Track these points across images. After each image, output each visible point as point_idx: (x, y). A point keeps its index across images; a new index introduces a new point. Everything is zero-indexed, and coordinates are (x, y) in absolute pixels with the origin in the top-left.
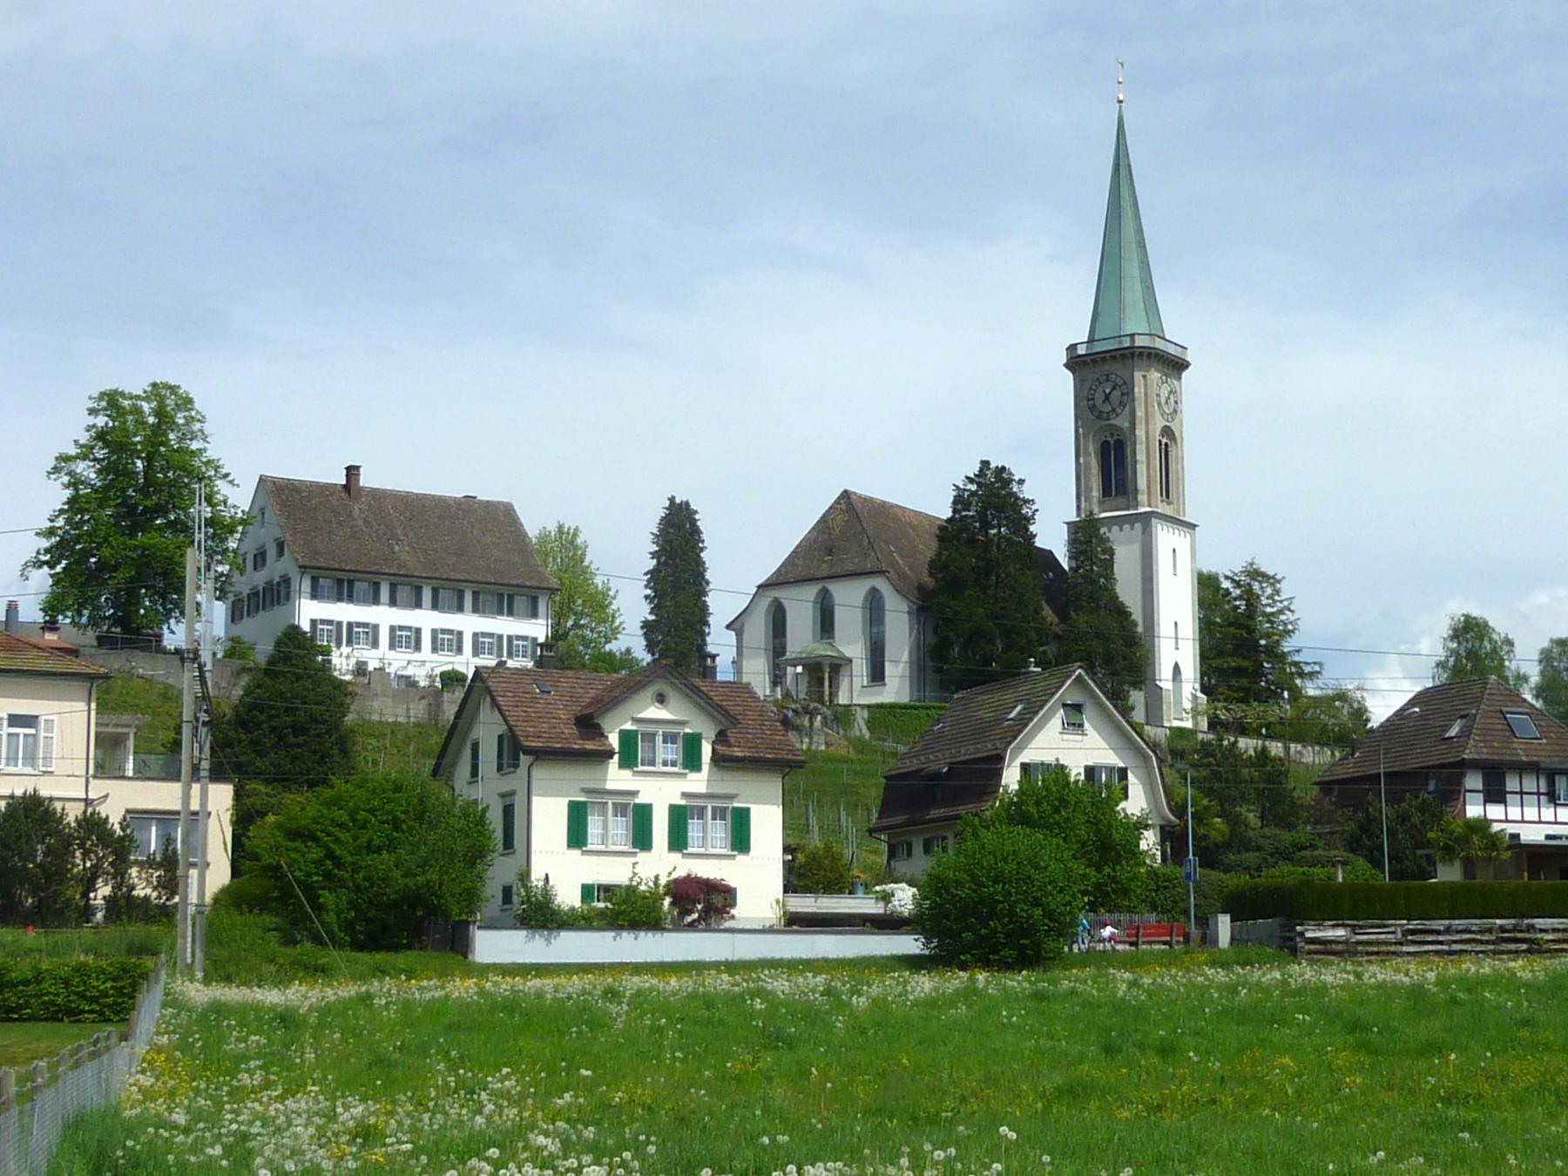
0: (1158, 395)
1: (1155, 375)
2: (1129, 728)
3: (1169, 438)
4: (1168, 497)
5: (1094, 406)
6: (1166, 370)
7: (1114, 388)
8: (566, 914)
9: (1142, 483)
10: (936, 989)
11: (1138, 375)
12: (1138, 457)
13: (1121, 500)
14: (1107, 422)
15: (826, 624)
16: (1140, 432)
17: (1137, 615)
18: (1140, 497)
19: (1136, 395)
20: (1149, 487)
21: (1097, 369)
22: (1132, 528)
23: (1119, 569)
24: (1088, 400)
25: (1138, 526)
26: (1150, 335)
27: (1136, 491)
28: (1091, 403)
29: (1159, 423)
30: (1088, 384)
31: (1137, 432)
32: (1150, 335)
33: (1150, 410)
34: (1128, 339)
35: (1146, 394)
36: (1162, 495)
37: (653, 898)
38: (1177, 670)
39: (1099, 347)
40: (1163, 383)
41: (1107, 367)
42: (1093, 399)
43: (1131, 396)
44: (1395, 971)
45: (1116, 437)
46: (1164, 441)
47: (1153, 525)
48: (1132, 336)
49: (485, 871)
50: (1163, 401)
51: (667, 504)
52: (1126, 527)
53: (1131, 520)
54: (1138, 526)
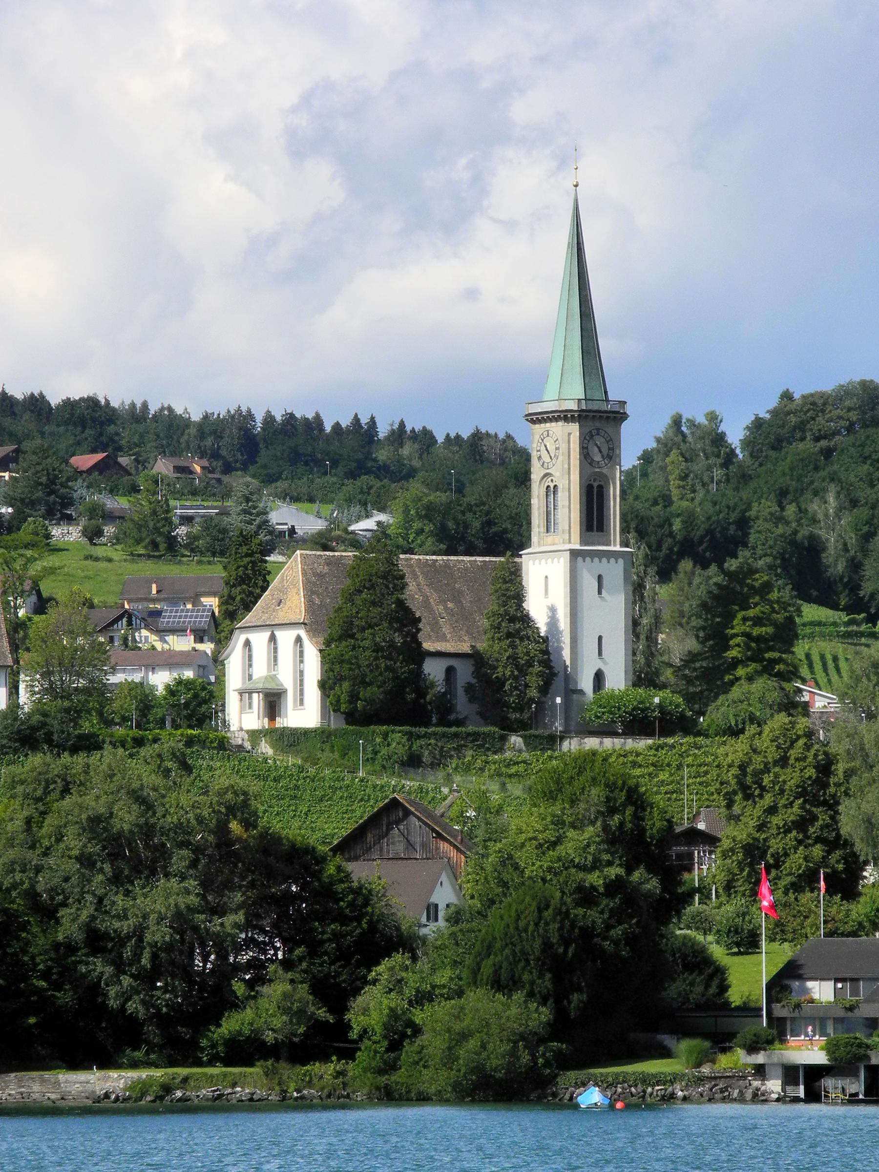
41: (548, 425)
42: (587, 448)
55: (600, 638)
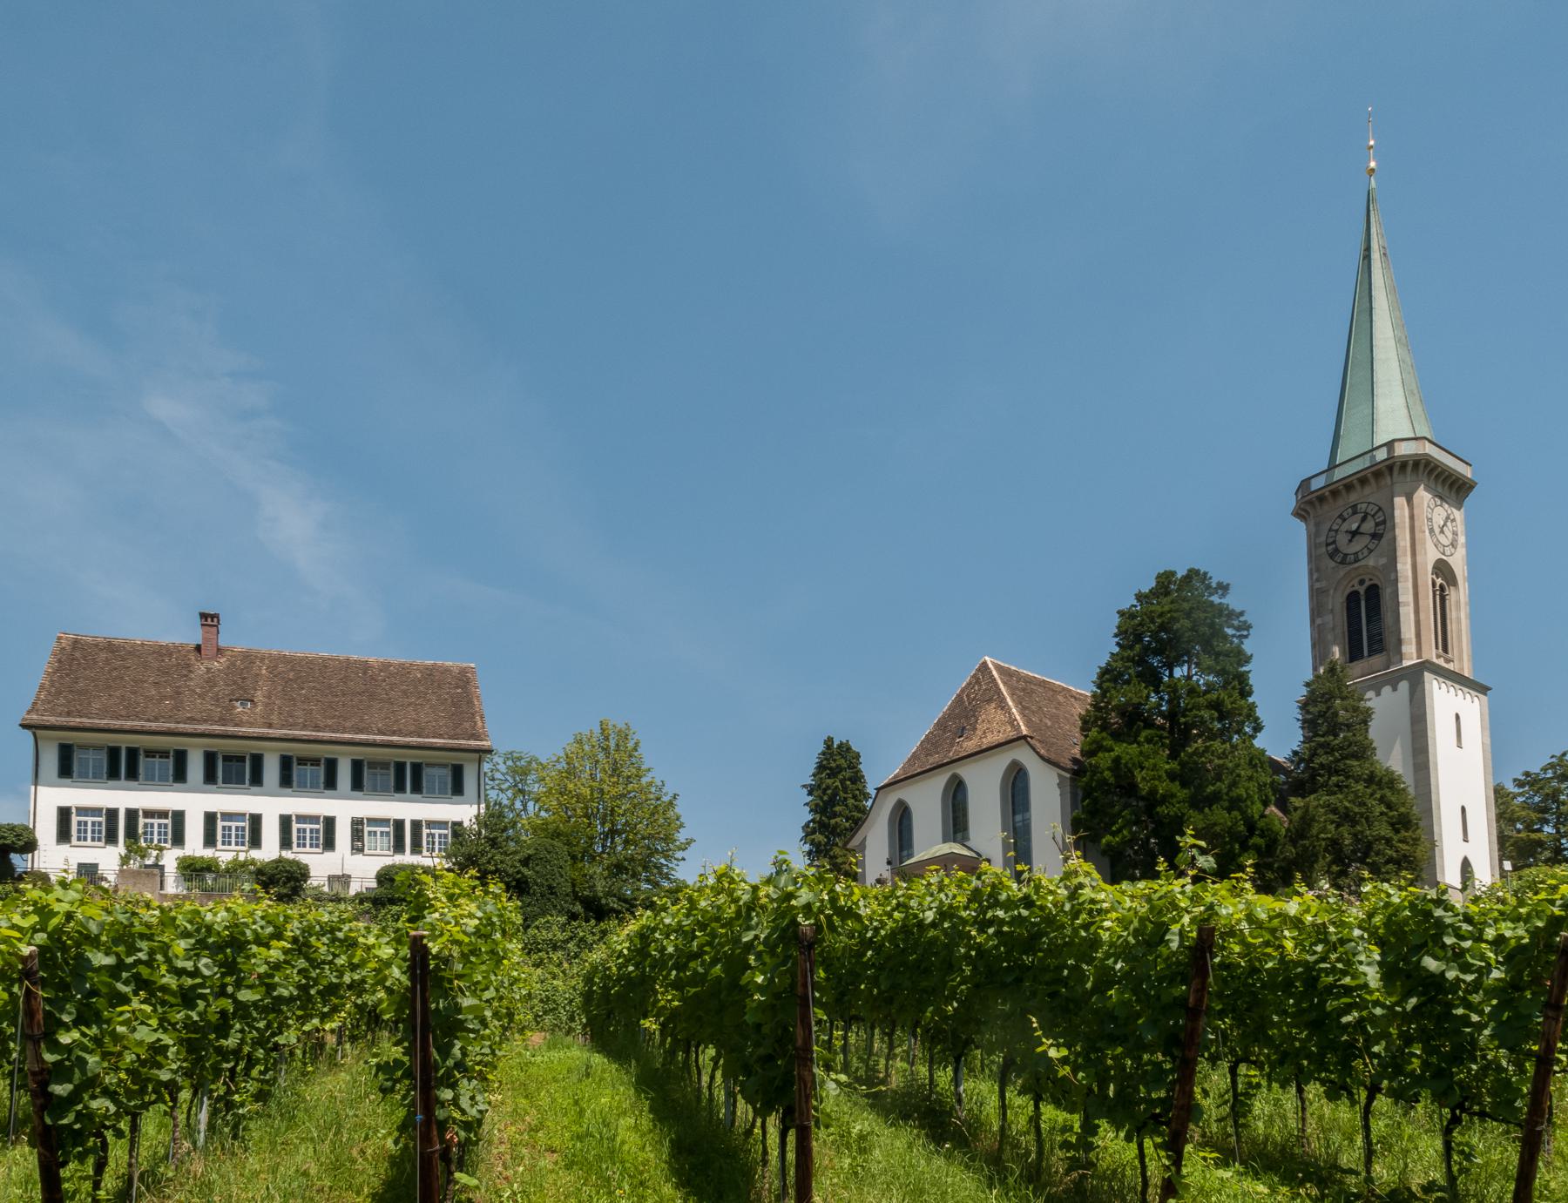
0: (1430, 520)
1: (1423, 496)
2: (1464, 633)
3: (1445, 579)
4: (1445, 650)
5: (1337, 550)
6: (1440, 489)
7: (1364, 519)
8: (385, 1191)
9: (1408, 631)
10: (1282, 1185)
11: (1400, 501)
12: (1401, 599)
13: (1377, 660)
14: (1357, 565)
15: (957, 822)
16: (1404, 566)
17: (1408, 780)
18: (1405, 649)
19: (1397, 520)
20: (1418, 635)
21: (1340, 502)
22: (1395, 689)
23: (1376, 732)
24: (1327, 545)
25: (1404, 686)
26: (1416, 439)
27: (1399, 642)
28: (1330, 548)
29: (1430, 555)
30: (1326, 527)
31: (1399, 566)
32: (1416, 439)
33: (1418, 535)
34: (1385, 449)
35: (1412, 517)
36: (1437, 648)
37: (101, 1175)
38: (1466, 866)
39: (1339, 474)
40: (1436, 506)
41: (1353, 497)
42: (1334, 542)
43: (1388, 524)
44: (499, 962)
45: (1367, 583)
46: (1439, 581)
47: (1426, 680)
48: (1390, 445)
49: (1275, 1143)
50: (1437, 530)
51: (821, 748)
52: (1387, 690)
53: (1393, 681)
54: (1404, 686)
55: (1463, 809)
